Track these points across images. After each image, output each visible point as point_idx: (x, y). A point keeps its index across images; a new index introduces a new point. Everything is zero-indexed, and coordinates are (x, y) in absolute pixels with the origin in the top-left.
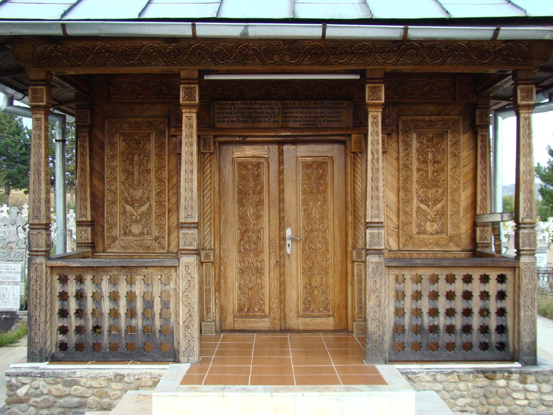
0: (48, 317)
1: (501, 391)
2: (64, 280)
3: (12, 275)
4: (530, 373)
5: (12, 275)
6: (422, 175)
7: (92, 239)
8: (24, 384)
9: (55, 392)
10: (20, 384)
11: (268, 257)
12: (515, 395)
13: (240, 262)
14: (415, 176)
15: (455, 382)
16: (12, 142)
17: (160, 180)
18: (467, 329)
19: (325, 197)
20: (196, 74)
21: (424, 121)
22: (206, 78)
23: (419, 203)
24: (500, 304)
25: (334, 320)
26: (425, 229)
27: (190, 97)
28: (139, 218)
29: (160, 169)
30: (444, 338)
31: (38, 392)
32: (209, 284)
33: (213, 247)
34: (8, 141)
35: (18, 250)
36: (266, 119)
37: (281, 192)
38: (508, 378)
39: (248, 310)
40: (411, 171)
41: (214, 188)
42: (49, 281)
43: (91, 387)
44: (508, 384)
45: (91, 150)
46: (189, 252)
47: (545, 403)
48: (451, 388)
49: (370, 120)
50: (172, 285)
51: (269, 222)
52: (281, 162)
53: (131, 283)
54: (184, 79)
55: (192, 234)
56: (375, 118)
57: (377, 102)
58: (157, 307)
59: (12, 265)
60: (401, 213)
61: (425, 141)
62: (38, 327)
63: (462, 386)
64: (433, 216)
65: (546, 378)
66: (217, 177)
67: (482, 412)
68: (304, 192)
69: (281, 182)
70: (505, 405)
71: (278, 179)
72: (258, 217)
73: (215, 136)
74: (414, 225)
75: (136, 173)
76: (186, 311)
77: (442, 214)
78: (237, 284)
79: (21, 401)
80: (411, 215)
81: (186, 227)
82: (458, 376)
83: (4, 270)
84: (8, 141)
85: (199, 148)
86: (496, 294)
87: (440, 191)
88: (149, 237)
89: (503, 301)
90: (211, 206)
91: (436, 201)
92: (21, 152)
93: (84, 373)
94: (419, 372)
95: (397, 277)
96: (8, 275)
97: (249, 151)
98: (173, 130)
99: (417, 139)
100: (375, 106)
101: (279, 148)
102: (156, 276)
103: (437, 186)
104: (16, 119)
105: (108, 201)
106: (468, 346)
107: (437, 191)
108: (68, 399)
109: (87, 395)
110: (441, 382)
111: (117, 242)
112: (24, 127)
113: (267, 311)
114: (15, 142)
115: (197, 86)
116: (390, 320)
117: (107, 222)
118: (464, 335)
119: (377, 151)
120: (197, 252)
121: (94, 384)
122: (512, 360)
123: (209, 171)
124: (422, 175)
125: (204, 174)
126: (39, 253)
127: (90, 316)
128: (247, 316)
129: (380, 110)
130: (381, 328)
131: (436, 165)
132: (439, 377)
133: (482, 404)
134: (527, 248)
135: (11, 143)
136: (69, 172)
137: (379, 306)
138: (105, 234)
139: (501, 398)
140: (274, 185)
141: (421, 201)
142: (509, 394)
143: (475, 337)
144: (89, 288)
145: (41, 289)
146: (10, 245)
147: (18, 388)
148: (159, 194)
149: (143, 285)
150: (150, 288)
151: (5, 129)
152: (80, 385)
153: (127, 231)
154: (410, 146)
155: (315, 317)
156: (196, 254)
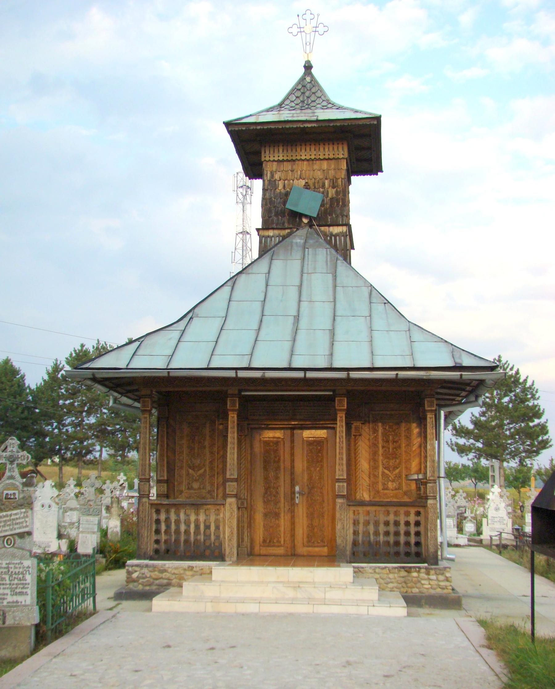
0: (149, 533)
1: (414, 579)
2: (158, 512)
3: (91, 526)
4: (432, 569)
5: (91, 526)
6: (386, 450)
7: (167, 491)
8: (136, 571)
9: (154, 576)
10: (133, 571)
11: (283, 505)
12: (423, 582)
13: (264, 509)
14: (381, 451)
15: (387, 574)
16: (13, 404)
17: (212, 453)
18: (397, 543)
19: (321, 465)
20: (237, 392)
21: (387, 414)
22: (243, 393)
23: (384, 469)
24: (417, 529)
25: (328, 550)
26: (388, 487)
27: (233, 404)
28: (197, 478)
29: (212, 445)
30: (384, 549)
31: (144, 576)
32: (244, 522)
33: (246, 498)
34: (8, 403)
35: (96, 507)
36: (281, 414)
37: (293, 461)
38: (419, 572)
39: (270, 541)
40: (378, 447)
41: (247, 459)
42: (150, 512)
43: (174, 574)
44: (419, 575)
45: (167, 433)
46: (232, 496)
47: (441, 587)
48: (385, 577)
49: (338, 419)
50: (221, 515)
51: (284, 481)
52: (292, 441)
53: (197, 514)
54: (230, 395)
55: (234, 485)
56: (341, 417)
57: (342, 408)
58: (213, 528)
59: (91, 518)
60: (372, 476)
61: (387, 428)
62: (143, 539)
63: (391, 576)
64: (393, 478)
65: (442, 572)
66: (249, 452)
67: (403, 592)
68: (308, 461)
69: (292, 454)
70: (417, 588)
71: (290, 452)
72: (277, 478)
73: (248, 424)
74: (380, 484)
75: (196, 448)
76: (230, 530)
77: (399, 476)
78: (262, 524)
79: (134, 581)
80: (378, 477)
81: (230, 481)
82: (389, 570)
83: (85, 522)
84: (9, 403)
85: (238, 433)
86: (414, 522)
87: (398, 461)
88: (204, 491)
89: (419, 527)
90: (245, 471)
91: (395, 468)
92: (23, 416)
93: (171, 565)
94: (366, 567)
95: (354, 511)
96: (87, 526)
97: (269, 435)
98: (221, 420)
99: (382, 426)
100: (341, 410)
101: (291, 432)
102: (212, 509)
103: (396, 458)
104: (18, 377)
105: (178, 467)
106: (397, 554)
107: (396, 461)
108: (161, 581)
109: (172, 578)
110: (379, 574)
111: (183, 494)
112: (26, 386)
113: (282, 542)
114: (17, 404)
115: (237, 399)
116: (350, 537)
117: (177, 480)
118: (395, 547)
119: (342, 437)
120: (236, 496)
121: (176, 571)
122: (424, 563)
123: (244, 447)
124: (386, 450)
125: (241, 449)
126: (145, 496)
127: (173, 534)
128: (268, 546)
129: (344, 413)
130: (344, 542)
131: (395, 444)
132: (377, 570)
133: (403, 587)
134: (432, 495)
135: (11, 405)
136: (78, 440)
137: (343, 528)
138: (176, 488)
139: (415, 583)
140: (288, 457)
141: (385, 468)
142: (419, 582)
143: (402, 549)
144: (173, 517)
145: (145, 517)
146: (89, 503)
147: (132, 573)
148: (211, 462)
149: (204, 515)
150: (208, 517)
151: (5, 389)
152: (168, 572)
153: (190, 487)
154: (378, 431)
155: (315, 547)
156: (235, 497)
